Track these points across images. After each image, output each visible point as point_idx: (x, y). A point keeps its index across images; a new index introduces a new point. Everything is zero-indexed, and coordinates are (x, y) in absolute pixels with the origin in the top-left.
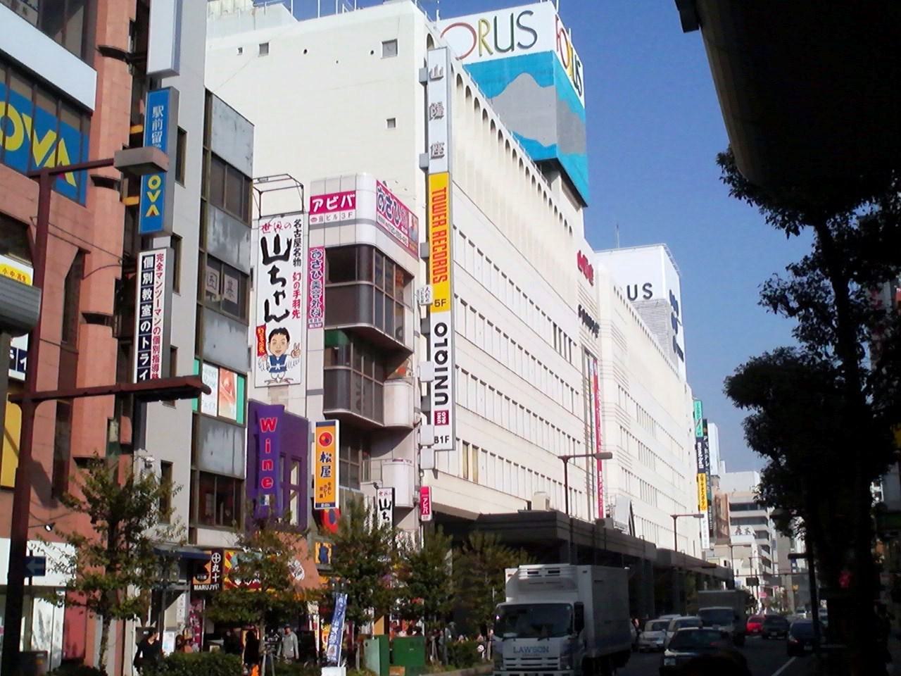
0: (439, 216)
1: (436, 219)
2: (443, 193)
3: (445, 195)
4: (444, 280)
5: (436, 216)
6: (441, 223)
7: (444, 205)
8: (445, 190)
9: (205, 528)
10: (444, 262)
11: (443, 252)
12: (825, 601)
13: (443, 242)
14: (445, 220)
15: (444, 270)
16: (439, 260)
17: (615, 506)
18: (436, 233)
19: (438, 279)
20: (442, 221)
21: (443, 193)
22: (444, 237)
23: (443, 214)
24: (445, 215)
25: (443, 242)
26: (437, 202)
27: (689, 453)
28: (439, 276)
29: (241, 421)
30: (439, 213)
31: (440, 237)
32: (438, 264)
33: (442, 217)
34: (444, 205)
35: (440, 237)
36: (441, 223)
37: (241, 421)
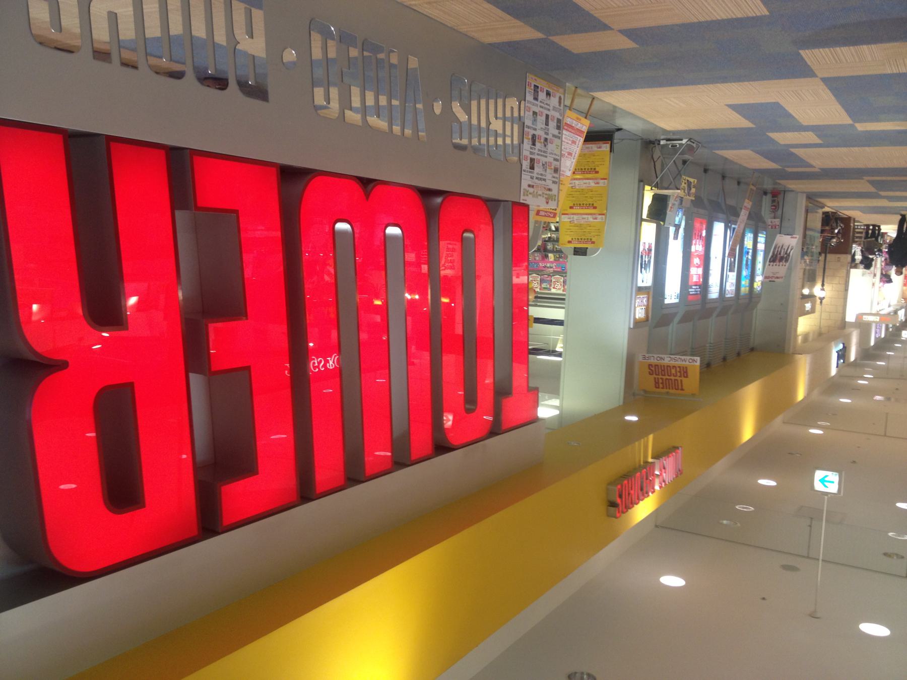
0: (662, 383)
1: (660, 381)
2: (680, 387)
3: (678, 389)
4: (650, 372)
5: (663, 381)
6: (657, 385)
7: (671, 388)
8: (682, 389)
9: (272, 633)
10: (663, 374)
11: (671, 374)
12: (451, 417)
13: (678, 374)
14: (658, 388)
15: (657, 373)
16: (666, 370)
17: (820, 254)
18: (686, 370)
19: (651, 368)
20: (659, 385)
21: (680, 387)
22: (682, 376)
23: (663, 386)
24: (663, 388)
25: (678, 374)
26: (673, 382)
27: (643, 281)
28: (653, 369)
29: (367, 475)
30: (664, 384)
31: (682, 372)
32: (663, 369)
33: (661, 386)
34: (671, 388)
35: (682, 372)
36: (657, 385)
37: (367, 475)
